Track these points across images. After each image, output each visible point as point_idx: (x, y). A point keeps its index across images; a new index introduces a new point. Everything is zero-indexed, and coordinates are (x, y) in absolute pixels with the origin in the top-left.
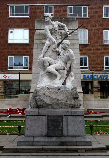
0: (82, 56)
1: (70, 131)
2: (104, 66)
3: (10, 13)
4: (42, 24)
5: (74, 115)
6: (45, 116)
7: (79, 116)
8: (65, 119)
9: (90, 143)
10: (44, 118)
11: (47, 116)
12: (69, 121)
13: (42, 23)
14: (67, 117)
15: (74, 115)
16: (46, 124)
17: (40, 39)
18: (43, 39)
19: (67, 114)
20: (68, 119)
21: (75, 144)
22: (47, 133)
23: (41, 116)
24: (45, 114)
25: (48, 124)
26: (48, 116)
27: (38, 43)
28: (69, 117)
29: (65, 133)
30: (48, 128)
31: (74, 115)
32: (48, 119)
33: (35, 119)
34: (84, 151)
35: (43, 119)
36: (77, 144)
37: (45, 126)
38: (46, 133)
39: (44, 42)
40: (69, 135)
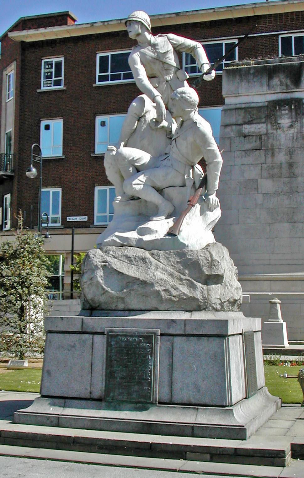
0: (120, 73)
1: (177, 386)
2: (98, 74)
3: (186, 64)
4: (242, 80)
5: (193, 335)
6: (102, 333)
7: (212, 339)
8: (160, 347)
9: (238, 433)
10: (100, 341)
11: (108, 334)
12: (176, 352)
13: (249, 82)
14: (168, 340)
15: (193, 335)
16: (105, 361)
17: (236, 125)
18: (245, 123)
19: (171, 331)
20: (175, 345)
21: (189, 431)
22: (108, 390)
23: (91, 336)
24: (101, 328)
25: (109, 362)
26: (111, 336)
27: (232, 134)
28: (177, 340)
29: (159, 390)
30: (110, 375)
31: (195, 332)
32: (109, 344)
33: (73, 344)
34: (208, 456)
35: (96, 345)
36: (196, 432)
37: (101, 368)
38: (104, 389)
39: (249, 132)
40: (176, 402)
